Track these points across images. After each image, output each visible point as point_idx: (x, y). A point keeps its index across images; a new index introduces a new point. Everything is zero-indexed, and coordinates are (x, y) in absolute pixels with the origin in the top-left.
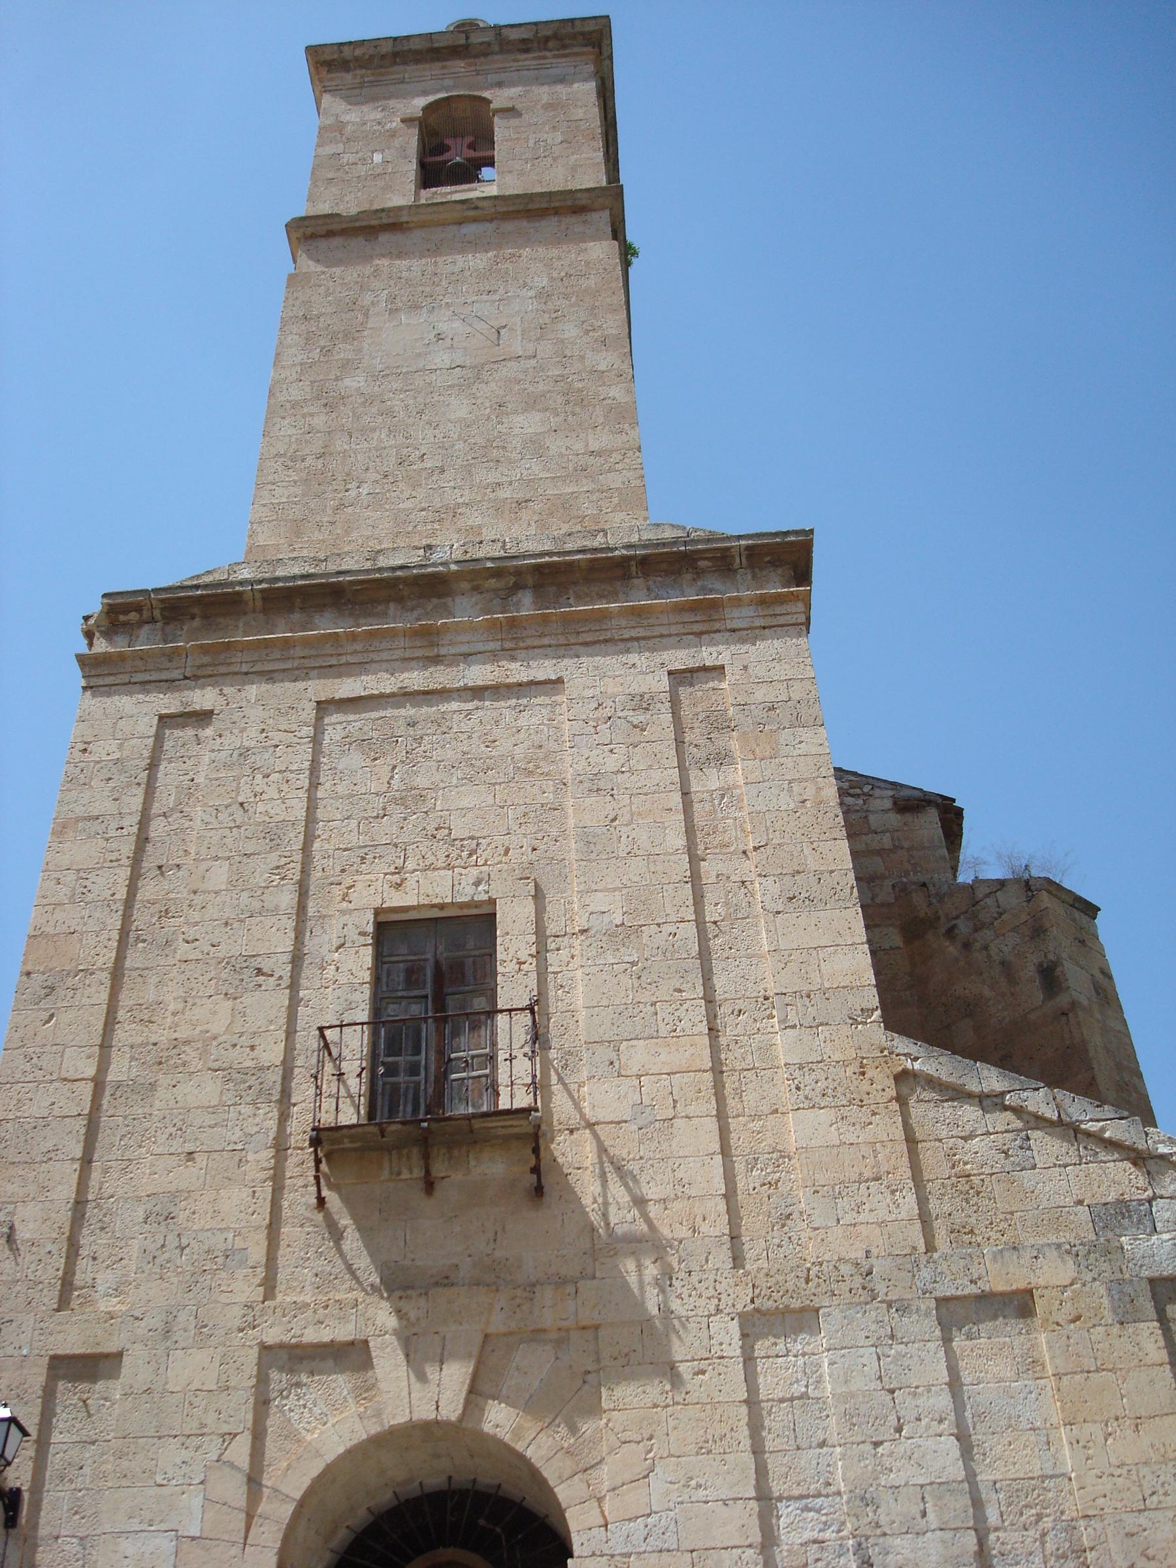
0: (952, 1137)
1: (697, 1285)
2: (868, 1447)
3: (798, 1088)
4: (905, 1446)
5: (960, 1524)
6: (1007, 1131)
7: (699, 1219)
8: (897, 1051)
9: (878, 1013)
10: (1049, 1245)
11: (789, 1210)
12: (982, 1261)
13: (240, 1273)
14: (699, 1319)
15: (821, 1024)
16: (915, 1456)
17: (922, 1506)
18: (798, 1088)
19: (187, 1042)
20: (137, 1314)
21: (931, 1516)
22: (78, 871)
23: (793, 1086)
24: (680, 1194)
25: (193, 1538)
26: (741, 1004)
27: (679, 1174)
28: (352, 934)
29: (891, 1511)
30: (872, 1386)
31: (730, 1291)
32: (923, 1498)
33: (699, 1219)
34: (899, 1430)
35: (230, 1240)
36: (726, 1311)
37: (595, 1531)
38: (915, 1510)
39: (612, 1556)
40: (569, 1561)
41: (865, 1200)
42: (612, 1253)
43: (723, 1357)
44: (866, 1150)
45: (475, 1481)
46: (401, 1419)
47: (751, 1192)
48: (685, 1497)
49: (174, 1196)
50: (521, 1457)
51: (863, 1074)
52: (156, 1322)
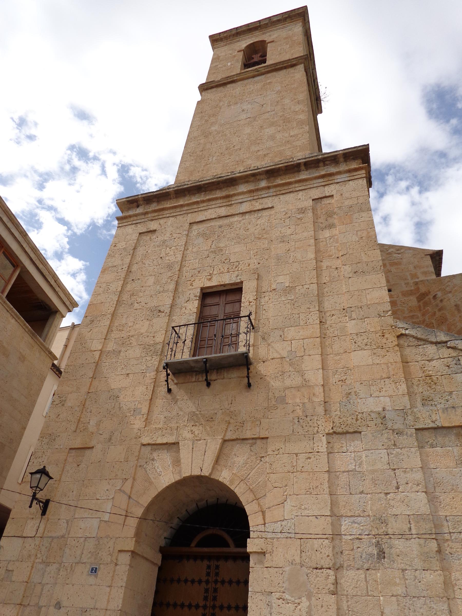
2: (382, 495)
4: (400, 496)
19: (132, 336)
20: (101, 432)
26: (333, 312)
34: (398, 488)
48: (299, 514)
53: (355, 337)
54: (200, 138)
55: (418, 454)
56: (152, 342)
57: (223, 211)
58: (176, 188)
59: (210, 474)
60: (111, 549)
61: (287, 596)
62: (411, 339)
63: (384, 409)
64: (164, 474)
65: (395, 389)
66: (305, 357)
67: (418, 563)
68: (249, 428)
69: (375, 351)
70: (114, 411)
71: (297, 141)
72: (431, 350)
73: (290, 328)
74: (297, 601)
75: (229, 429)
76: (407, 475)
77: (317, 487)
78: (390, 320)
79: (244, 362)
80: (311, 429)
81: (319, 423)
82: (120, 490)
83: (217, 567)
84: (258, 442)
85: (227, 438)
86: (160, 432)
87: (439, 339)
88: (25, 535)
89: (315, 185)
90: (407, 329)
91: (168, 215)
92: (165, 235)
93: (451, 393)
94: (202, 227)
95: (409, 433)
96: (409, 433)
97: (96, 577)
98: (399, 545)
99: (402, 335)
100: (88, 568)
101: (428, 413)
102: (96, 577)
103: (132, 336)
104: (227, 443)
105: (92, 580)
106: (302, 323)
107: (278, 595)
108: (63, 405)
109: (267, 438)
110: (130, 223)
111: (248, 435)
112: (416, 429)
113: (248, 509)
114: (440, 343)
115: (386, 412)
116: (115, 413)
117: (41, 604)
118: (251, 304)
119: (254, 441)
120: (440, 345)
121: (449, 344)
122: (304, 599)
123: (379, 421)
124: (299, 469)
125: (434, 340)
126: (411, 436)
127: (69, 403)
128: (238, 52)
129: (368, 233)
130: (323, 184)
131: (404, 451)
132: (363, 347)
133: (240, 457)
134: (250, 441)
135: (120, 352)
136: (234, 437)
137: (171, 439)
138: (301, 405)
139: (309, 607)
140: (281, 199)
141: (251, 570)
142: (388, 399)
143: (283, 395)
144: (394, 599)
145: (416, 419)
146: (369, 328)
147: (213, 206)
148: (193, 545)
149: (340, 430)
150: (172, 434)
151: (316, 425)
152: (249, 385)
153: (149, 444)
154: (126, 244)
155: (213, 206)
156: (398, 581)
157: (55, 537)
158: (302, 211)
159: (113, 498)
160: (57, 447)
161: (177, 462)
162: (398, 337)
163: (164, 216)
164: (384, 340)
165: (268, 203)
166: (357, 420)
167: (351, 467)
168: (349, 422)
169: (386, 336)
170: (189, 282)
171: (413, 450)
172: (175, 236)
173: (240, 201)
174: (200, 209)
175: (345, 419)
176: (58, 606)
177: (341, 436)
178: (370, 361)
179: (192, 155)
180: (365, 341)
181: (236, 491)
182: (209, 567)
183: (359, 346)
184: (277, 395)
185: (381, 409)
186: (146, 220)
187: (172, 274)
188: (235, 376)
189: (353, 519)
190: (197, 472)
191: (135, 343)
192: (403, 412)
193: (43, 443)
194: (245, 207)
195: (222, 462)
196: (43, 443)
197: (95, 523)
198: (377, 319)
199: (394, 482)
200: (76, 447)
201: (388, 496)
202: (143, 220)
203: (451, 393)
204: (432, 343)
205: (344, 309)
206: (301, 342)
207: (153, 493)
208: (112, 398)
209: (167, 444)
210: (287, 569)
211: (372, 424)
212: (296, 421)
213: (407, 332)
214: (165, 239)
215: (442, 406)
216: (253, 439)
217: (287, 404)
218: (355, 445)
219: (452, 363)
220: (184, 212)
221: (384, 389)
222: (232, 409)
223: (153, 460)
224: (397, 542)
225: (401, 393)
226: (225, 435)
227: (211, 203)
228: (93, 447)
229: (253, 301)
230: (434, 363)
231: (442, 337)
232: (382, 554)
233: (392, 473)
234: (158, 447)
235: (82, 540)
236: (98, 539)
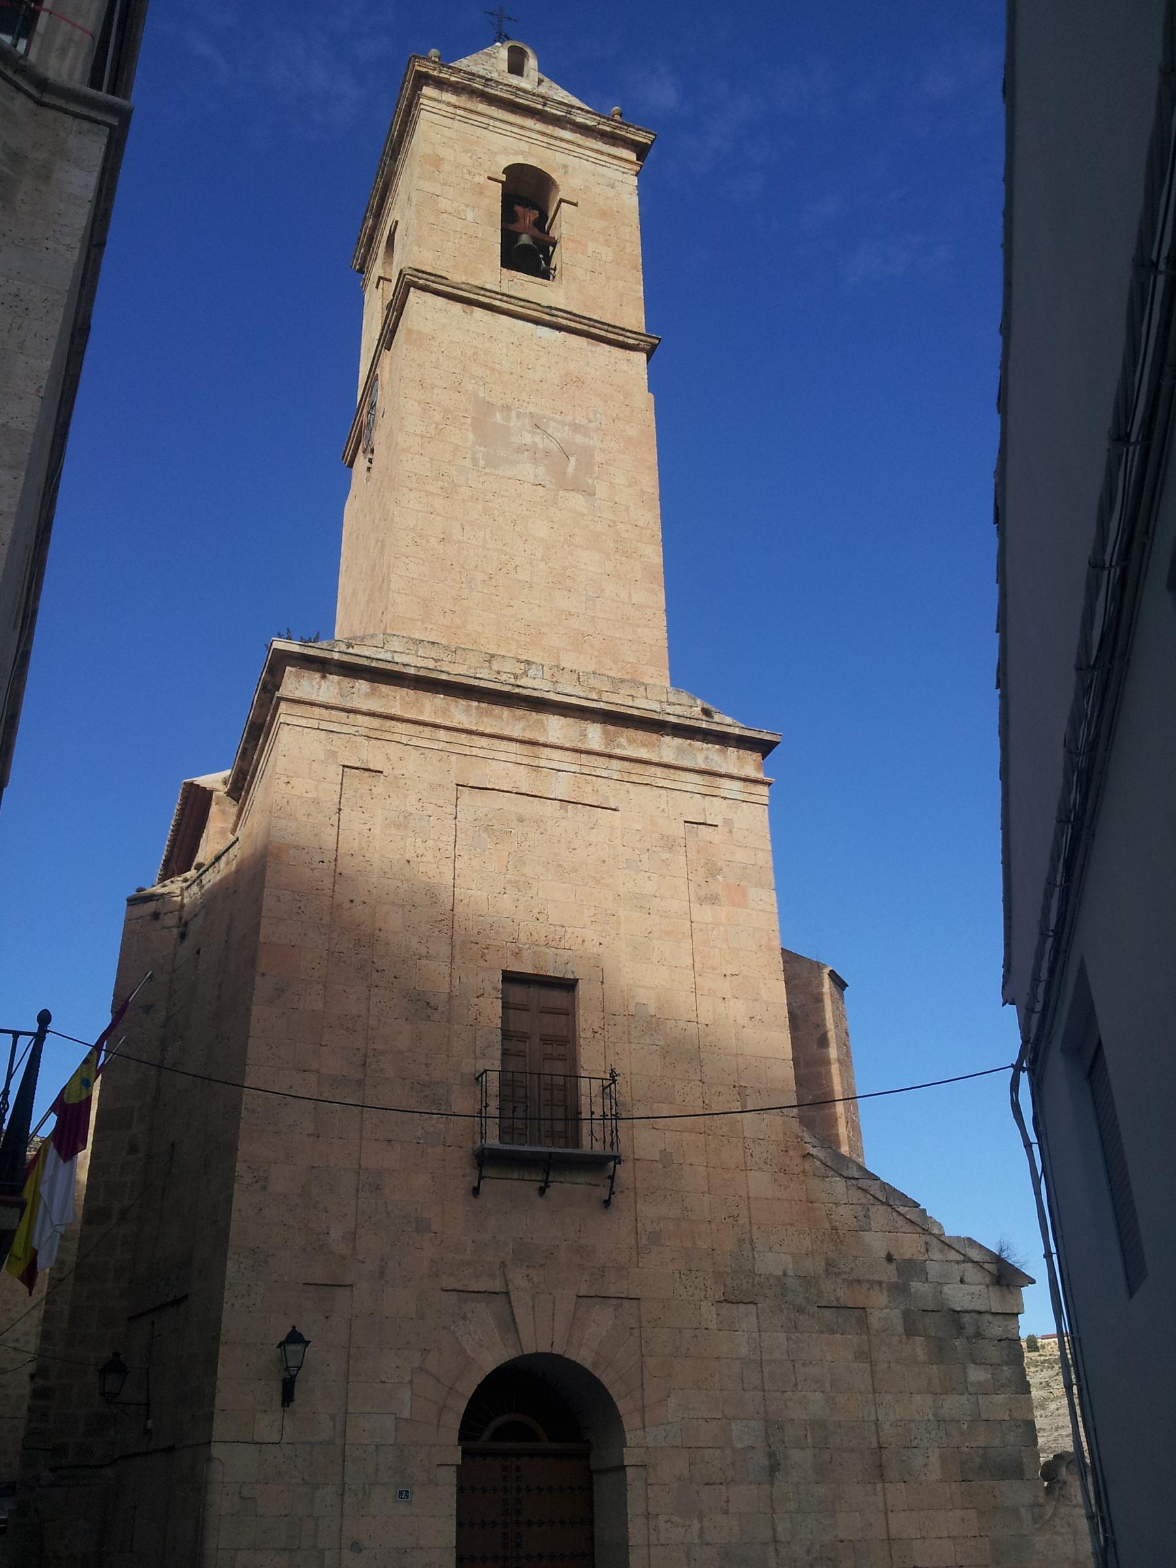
2: (779, 1394)
20: (361, 1257)
21: (809, 1440)
26: (720, 1088)
34: (796, 1385)
37: (638, 1432)
53: (751, 1145)
54: (432, 488)
56: (427, 1078)
57: (523, 779)
58: (422, 673)
61: (676, 1519)
62: (818, 1163)
63: (785, 1274)
71: (645, 626)
74: (687, 1523)
79: (601, 1165)
81: (708, 1283)
82: (420, 1368)
83: (518, 1468)
84: (626, 1303)
88: (258, 1439)
89: (689, 787)
91: (404, 740)
92: (406, 796)
94: (480, 798)
97: (410, 1503)
102: (410, 1503)
107: (665, 1517)
108: (264, 1188)
110: (315, 724)
111: (612, 1291)
118: (597, 1035)
119: (619, 1301)
120: (850, 1182)
122: (696, 1521)
125: (845, 1174)
128: (489, 178)
129: (770, 940)
130: (703, 790)
133: (601, 1323)
134: (614, 1301)
135: (726, 1512)
137: (497, 1285)
139: (701, 1529)
140: (632, 795)
141: (629, 1487)
142: (789, 1259)
144: (786, 1516)
145: (820, 1293)
147: (502, 756)
148: (487, 1434)
149: (732, 1298)
152: (607, 1203)
154: (316, 788)
155: (502, 756)
158: (669, 844)
159: (411, 1382)
161: (510, 1325)
163: (396, 737)
165: (608, 792)
166: (753, 1285)
169: (791, 1153)
170: (475, 947)
172: (430, 809)
173: (556, 766)
174: (475, 751)
176: (356, 1547)
177: (733, 1306)
179: (417, 539)
180: (765, 1155)
181: (602, 1380)
182: (505, 1468)
185: (780, 1273)
186: (353, 730)
190: (544, 1348)
192: (807, 1281)
193: (242, 1266)
194: (561, 787)
196: (242, 1266)
202: (345, 729)
204: (841, 1176)
212: (677, 1275)
214: (409, 809)
218: (746, 1318)
220: (441, 745)
223: (464, 1318)
227: (497, 742)
229: (600, 1031)
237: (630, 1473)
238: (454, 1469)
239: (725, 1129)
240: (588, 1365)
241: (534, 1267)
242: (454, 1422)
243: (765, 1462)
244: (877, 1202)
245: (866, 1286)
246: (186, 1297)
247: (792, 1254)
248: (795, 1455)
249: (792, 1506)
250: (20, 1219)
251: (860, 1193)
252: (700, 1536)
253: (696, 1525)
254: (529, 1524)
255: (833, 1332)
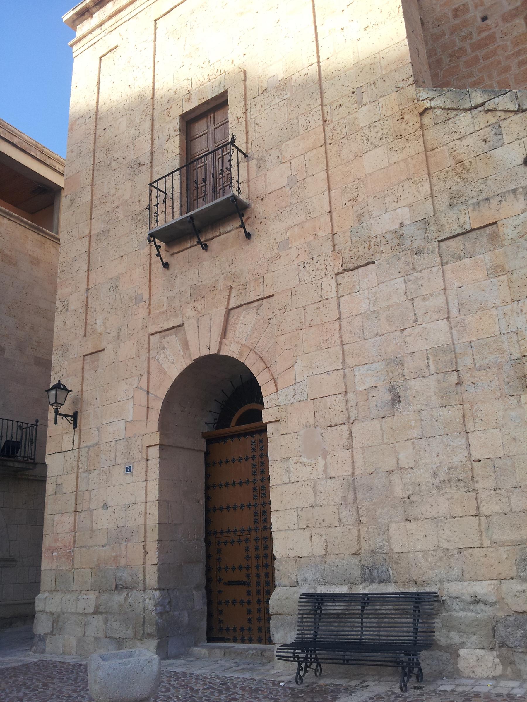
0: (454, 140)
1: (316, 264)
2: (398, 333)
3: (367, 140)
4: (418, 329)
5: (448, 370)
6: (486, 127)
7: (317, 229)
8: (422, 99)
9: (74, 56)
10: (508, 192)
11: (362, 211)
12: (467, 212)
13: (141, 304)
14: (316, 282)
15: (381, 97)
16: (424, 334)
17: (426, 361)
18: (367, 140)
19: (117, 207)
20: (108, 331)
21: (432, 367)
22: (78, 143)
23: (365, 139)
24: (308, 218)
25: (130, 421)
26: (340, 102)
27: (308, 207)
28: (172, 132)
29: (410, 365)
30: (402, 299)
31: (331, 264)
32: (427, 357)
33: (317, 229)
34: (416, 321)
35: (137, 291)
36: (329, 275)
37: (273, 396)
38: (423, 364)
39: (280, 406)
40: (263, 411)
41: (401, 194)
42: (278, 257)
43: (328, 299)
44: (402, 165)
45: (205, 247)
46: (197, 357)
47: (344, 206)
48: (311, 374)
49: (117, 278)
50: (243, 365)
51: (403, 118)
52: (114, 334)
53: (367, 132)
55: (440, 274)
59: (219, 350)
60: (140, 447)
61: (304, 460)
62: (439, 112)
64: (173, 364)
65: (417, 194)
66: (308, 180)
67: (435, 401)
68: (252, 289)
69: (392, 145)
70: (116, 304)
72: (464, 120)
73: (288, 142)
74: (313, 462)
75: (232, 296)
76: (427, 303)
77: (327, 340)
78: (411, 91)
80: (318, 272)
84: (264, 301)
85: (231, 307)
86: (165, 316)
87: (474, 103)
90: (432, 99)
93: (486, 178)
95: (431, 249)
96: (431, 249)
97: (132, 475)
98: (415, 385)
99: (426, 109)
100: (124, 469)
101: (455, 216)
102: (132, 475)
103: (117, 207)
104: (232, 311)
105: (129, 478)
106: (302, 130)
107: (295, 459)
108: (67, 310)
109: (273, 295)
112: (439, 241)
113: (261, 379)
114: (475, 107)
115: (404, 228)
116: (118, 306)
117: (92, 508)
119: (260, 302)
121: (490, 105)
122: (320, 459)
123: (396, 241)
124: (307, 324)
125: (467, 106)
126: (433, 252)
127: (72, 307)
131: (424, 274)
132: (376, 143)
134: (256, 304)
136: (239, 304)
138: (306, 245)
139: (325, 466)
142: (406, 209)
143: (286, 237)
144: (409, 443)
145: (440, 228)
146: (384, 112)
149: (350, 266)
150: (176, 316)
151: (324, 267)
152: (248, 236)
153: (156, 333)
156: (413, 424)
157: (91, 446)
160: (71, 357)
162: (422, 114)
164: (404, 126)
166: (370, 248)
167: (364, 307)
168: (361, 253)
169: (406, 118)
171: (435, 269)
175: (355, 250)
178: (385, 164)
183: (372, 144)
184: (278, 240)
185: (397, 226)
187: (146, 106)
188: (230, 232)
189: (366, 366)
191: (121, 216)
192: (425, 222)
195: (230, 334)
197: (122, 424)
198: (394, 95)
199: (412, 314)
200: (89, 353)
201: (405, 333)
203: (486, 178)
204: (465, 110)
205: (353, 93)
206: (302, 159)
207: (168, 384)
208: (111, 289)
209: (173, 328)
210: (302, 433)
211: (388, 247)
213: (433, 103)
215: (474, 201)
216: (258, 300)
217: (290, 248)
219: (489, 133)
221: (402, 198)
222: (233, 271)
223: (164, 348)
224: (413, 383)
225: (422, 196)
226: (228, 304)
228: (104, 349)
230: (465, 142)
231: (478, 98)
232: (396, 399)
233: (409, 304)
234: (167, 332)
235: (113, 443)
236: (127, 439)
237: (270, 428)
238: (158, 447)
239: (344, 131)
240: (236, 356)
241: (198, 300)
242: (155, 416)
243: (388, 397)
244: (509, 114)
245: (494, 202)
246: (104, 349)
247: (410, 205)
248: (415, 385)
249: (415, 433)
250: (421, 19)
251: (489, 115)
252: (325, 471)
253: (321, 462)
254: (247, 482)
255: (460, 258)
